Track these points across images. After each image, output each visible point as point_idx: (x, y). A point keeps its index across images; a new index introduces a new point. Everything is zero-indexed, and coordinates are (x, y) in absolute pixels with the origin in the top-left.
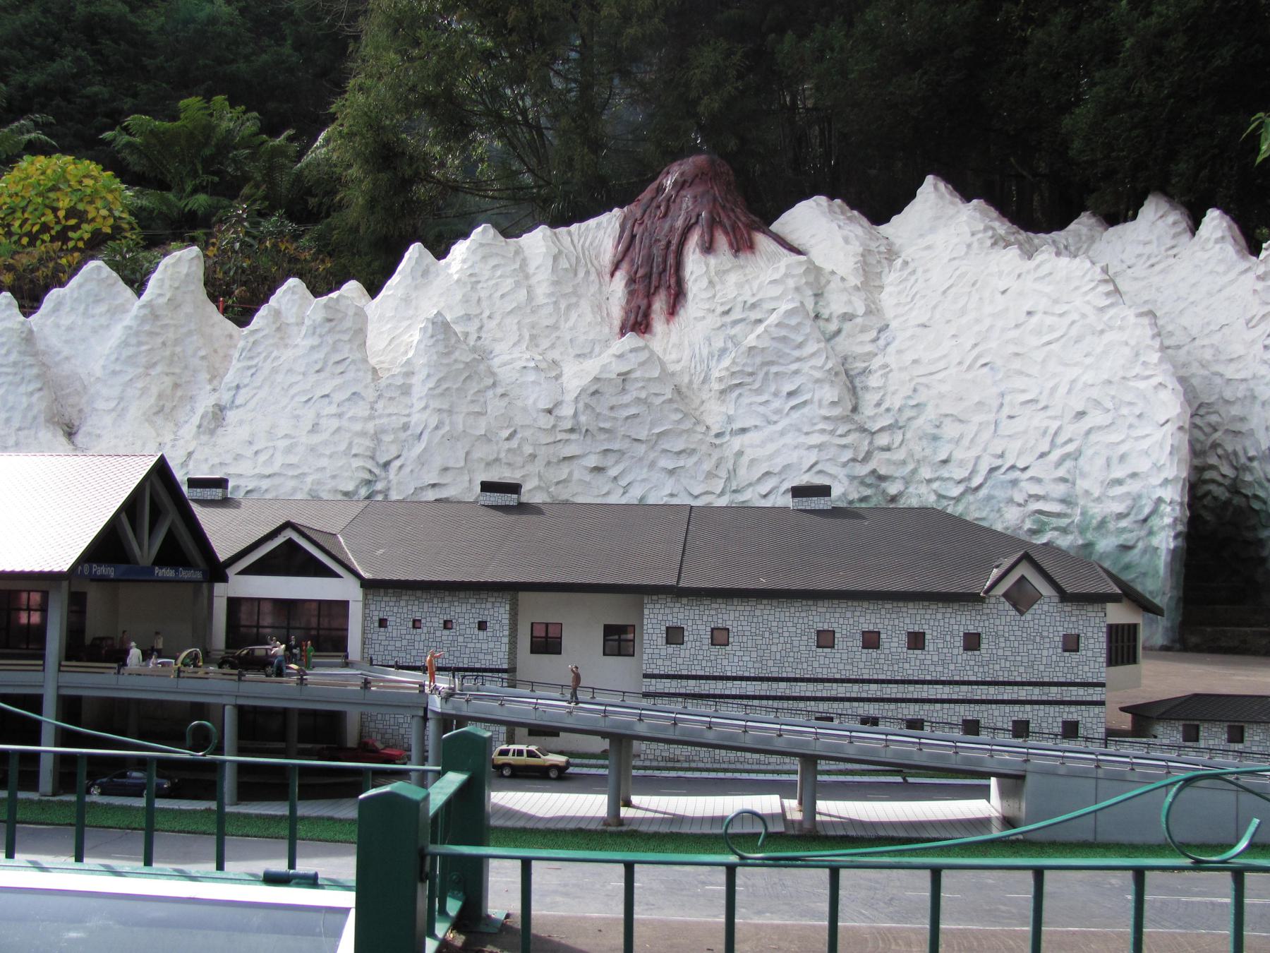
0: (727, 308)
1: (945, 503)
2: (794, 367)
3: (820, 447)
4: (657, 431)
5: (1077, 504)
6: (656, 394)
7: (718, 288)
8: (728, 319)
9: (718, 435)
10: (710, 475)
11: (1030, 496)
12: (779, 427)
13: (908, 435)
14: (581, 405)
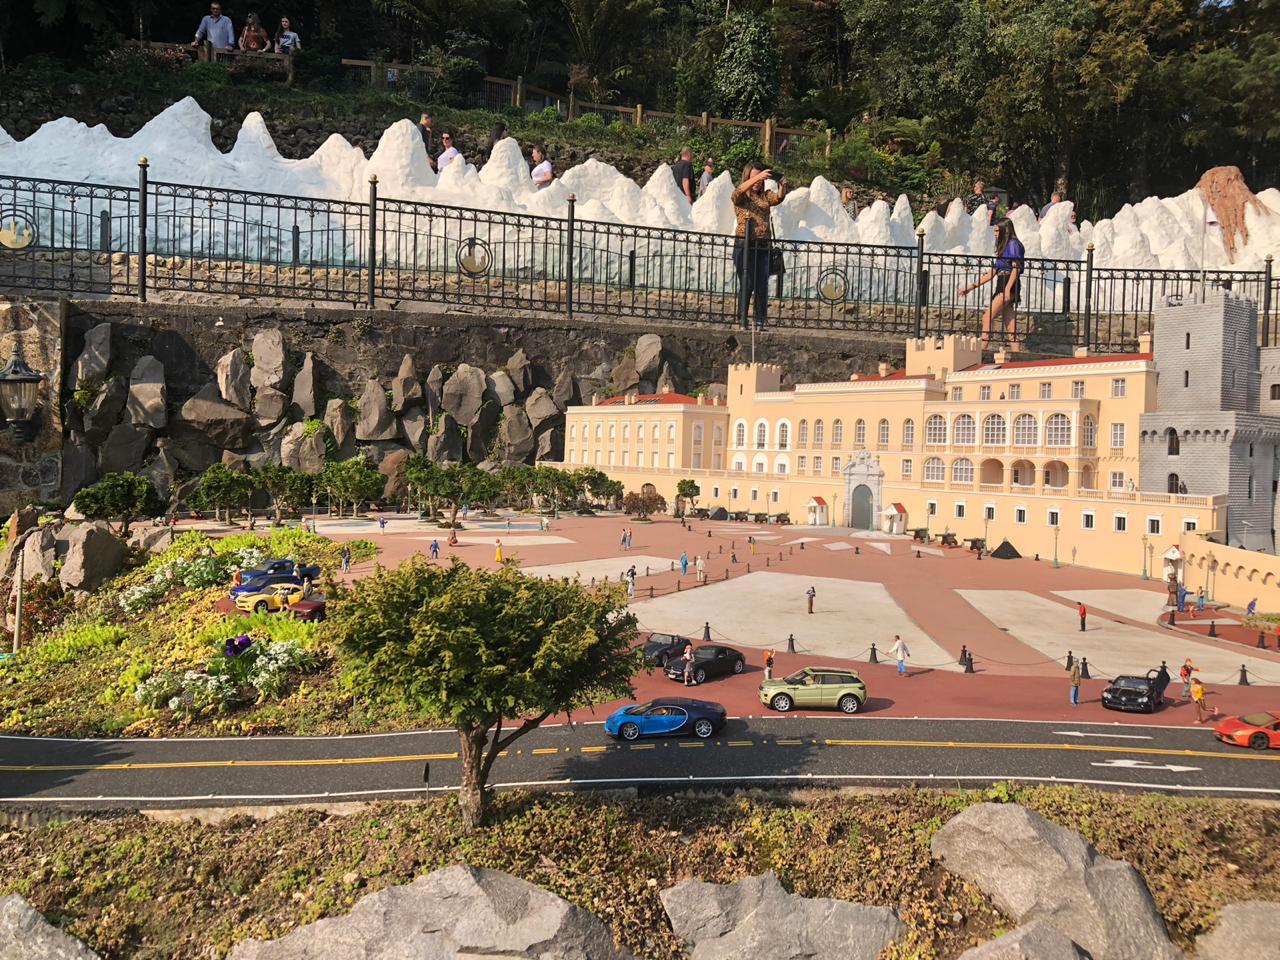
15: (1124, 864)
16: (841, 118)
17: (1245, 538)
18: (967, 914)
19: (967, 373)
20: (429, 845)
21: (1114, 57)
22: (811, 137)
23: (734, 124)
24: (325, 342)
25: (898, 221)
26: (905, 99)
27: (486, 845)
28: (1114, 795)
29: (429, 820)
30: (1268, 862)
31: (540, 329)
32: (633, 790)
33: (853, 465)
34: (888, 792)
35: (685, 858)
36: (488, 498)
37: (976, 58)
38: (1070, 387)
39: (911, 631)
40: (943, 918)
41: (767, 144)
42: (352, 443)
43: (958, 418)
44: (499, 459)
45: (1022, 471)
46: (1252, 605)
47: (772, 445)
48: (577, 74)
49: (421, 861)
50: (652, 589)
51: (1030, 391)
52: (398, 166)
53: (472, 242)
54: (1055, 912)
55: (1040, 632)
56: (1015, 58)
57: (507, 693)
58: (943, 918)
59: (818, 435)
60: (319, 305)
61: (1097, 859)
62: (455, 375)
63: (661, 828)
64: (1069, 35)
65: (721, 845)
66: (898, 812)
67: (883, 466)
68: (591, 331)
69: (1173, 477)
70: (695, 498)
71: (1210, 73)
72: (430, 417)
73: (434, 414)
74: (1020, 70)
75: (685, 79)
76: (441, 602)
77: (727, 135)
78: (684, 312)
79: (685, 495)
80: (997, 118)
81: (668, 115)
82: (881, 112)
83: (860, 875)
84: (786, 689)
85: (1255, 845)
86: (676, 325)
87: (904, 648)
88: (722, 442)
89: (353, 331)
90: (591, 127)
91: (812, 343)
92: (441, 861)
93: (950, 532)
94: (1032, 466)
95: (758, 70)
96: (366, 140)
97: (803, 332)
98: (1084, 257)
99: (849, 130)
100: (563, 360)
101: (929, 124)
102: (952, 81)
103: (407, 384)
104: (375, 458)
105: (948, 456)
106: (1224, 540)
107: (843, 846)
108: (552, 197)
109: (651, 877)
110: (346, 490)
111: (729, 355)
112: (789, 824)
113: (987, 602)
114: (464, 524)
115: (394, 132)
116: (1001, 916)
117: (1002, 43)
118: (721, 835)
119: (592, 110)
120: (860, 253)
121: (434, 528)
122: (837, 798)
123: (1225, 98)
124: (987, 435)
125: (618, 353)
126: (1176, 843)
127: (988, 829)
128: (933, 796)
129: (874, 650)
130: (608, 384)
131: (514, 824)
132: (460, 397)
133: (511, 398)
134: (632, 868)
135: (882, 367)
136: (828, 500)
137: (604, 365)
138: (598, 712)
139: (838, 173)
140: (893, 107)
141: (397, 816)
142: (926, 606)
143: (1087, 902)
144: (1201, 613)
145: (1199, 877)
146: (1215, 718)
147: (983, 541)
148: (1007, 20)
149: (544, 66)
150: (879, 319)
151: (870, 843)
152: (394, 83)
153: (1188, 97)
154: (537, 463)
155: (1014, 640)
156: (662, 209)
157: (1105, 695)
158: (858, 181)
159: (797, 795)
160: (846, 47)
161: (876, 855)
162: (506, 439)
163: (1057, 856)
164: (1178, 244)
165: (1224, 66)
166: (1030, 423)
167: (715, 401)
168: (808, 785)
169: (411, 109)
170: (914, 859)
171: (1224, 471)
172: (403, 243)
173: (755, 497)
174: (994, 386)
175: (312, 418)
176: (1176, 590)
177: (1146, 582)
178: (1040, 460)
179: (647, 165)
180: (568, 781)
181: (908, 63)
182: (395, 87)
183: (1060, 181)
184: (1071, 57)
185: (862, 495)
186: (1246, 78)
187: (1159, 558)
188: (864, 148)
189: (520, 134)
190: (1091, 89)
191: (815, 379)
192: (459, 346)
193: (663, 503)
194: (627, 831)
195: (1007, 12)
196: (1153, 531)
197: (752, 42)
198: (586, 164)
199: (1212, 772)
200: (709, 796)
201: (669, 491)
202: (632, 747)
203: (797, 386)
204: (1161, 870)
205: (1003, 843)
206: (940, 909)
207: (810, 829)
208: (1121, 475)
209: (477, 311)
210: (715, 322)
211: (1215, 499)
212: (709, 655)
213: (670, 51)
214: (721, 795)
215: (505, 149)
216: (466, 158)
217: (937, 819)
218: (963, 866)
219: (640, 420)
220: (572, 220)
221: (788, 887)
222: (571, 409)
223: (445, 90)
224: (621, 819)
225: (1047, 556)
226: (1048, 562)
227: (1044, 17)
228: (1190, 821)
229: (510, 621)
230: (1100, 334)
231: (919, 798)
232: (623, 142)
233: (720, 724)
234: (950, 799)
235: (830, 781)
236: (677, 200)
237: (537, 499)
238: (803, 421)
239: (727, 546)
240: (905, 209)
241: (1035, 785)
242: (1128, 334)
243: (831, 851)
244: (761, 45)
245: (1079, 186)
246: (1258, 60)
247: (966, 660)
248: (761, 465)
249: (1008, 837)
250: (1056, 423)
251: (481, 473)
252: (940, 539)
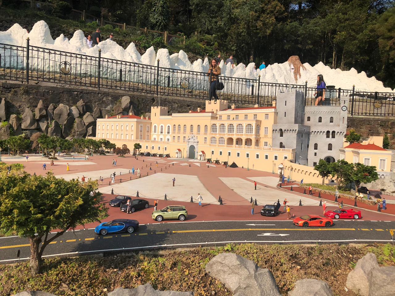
15: (267, 270)
16: (188, 33)
17: (300, 161)
18: (216, 291)
19: (223, 111)
20: (18, 282)
21: (266, 22)
22: (179, 38)
23: (155, 32)
24: (10, 95)
25: (205, 65)
26: (208, 29)
27: (40, 281)
28: (264, 246)
29: (19, 272)
30: (309, 265)
31: (88, 93)
32: (102, 255)
33: (190, 139)
34: (192, 249)
35: (119, 279)
36: (68, 149)
37: (228, 18)
38: (253, 116)
39: (204, 192)
40: (208, 294)
41: (166, 39)
42: (20, 130)
43: (221, 125)
44: (74, 136)
45: (239, 141)
46: (302, 181)
47: (165, 132)
48: (104, 11)
49: (13, 288)
50: (121, 180)
51: (242, 117)
52: (40, 36)
53: (65, 63)
54: (245, 288)
55: (244, 191)
56: (239, 19)
57: (44, 224)
58: (208, 294)
59: (179, 130)
60: (8, 82)
61: (258, 269)
62: (58, 107)
63: (111, 268)
64: (254, 14)
65: (132, 273)
66: (195, 256)
67: (198, 140)
68: (106, 94)
69: (281, 143)
70: (140, 149)
71: (291, 29)
72: (49, 121)
73: (50, 120)
74: (240, 23)
75: (140, 16)
76: (15, 190)
77: (153, 35)
78: (138, 90)
79: (137, 148)
80: (234, 37)
81: (134, 27)
82: (200, 32)
83: (181, 281)
84: (161, 214)
85: (305, 259)
86: (136, 93)
87: (201, 197)
88: (149, 131)
89: (21, 91)
90: (109, 29)
91: (178, 101)
92: (22, 288)
93: (218, 160)
94: (242, 140)
95: (163, 15)
96: (28, 26)
97: (176, 98)
98: (258, 79)
99: (191, 37)
100: (97, 103)
101: (215, 37)
102: (221, 24)
103: (41, 110)
104: (29, 135)
105: (217, 137)
106: (294, 162)
107: (176, 270)
108: (94, 51)
109: (105, 287)
110: (15, 146)
111: (152, 104)
112: (157, 263)
113: (227, 181)
114: (58, 158)
115: (38, 24)
116: (228, 291)
117: (236, 14)
118: (132, 269)
119: (109, 24)
120: (193, 74)
121: (47, 159)
122: (175, 252)
123: (295, 36)
124: (229, 130)
125: (115, 102)
126: (282, 261)
127: (224, 262)
128: (207, 250)
129: (192, 198)
130: (112, 112)
131: (52, 272)
132: (60, 115)
133: (78, 115)
134: (98, 285)
135: (199, 109)
136: (182, 150)
137: (111, 106)
138: (88, 228)
139: (187, 49)
140: (204, 31)
141: (6, 271)
142: (211, 185)
143: (255, 285)
144: (288, 183)
145: (289, 271)
146: (293, 217)
147: (227, 162)
148: (237, 8)
149: (93, 8)
150: (199, 95)
151: (185, 268)
152: (39, 8)
153: (286, 35)
154: (86, 137)
155: (236, 193)
156: (131, 57)
157: (262, 211)
158: (194, 53)
159: (161, 252)
160: (190, 11)
161: (187, 273)
162: (76, 129)
163: (246, 270)
164: (283, 77)
165: (296, 27)
166: (241, 127)
167: (147, 118)
168: (165, 248)
169: (45, 17)
170: (200, 273)
171: (295, 142)
172: (38, 62)
173: (159, 149)
174: (231, 116)
175: (5, 121)
176: (282, 177)
177: (273, 174)
178: (244, 138)
179: (127, 43)
180: (77, 252)
181: (208, 18)
182: (39, 9)
183: (251, 57)
184: (255, 20)
185: (192, 148)
186: (301, 31)
187: (277, 167)
188: (195, 43)
189: (84, 29)
190: (260, 30)
191: (179, 112)
192: (60, 98)
193: (129, 151)
194: (98, 270)
195: (237, 5)
196: (275, 159)
197: (161, 6)
198: (106, 40)
199: (293, 235)
200: (130, 255)
201: (131, 148)
202: (104, 238)
203: (173, 114)
204: (277, 270)
205: (229, 266)
206: (208, 291)
207: (164, 265)
208: (267, 142)
209: (67, 86)
210: (148, 93)
211: (292, 150)
212: (136, 203)
213: (135, 7)
214: (134, 254)
215: (78, 33)
216: (65, 36)
217: (208, 259)
218: (216, 275)
219: (122, 124)
220: (100, 58)
221: (155, 287)
222: (98, 120)
223: (57, 12)
224: (96, 266)
225: (246, 167)
226: (246, 168)
227: (247, 8)
228: (286, 253)
229: (47, 197)
230: (261, 102)
231: (202, 251)
232: (119, 35)
233: (137, 228)
234: (212, 251)
235: (173, 246)
236: (137, 54)
237: (86, 150)
238: (174, 125)
239: (149, 165)
240: (207, 62)
241: (240, 244)
242: (269, 102)
243: (171, 273)
244: (164, 8)
245: (256, 58)
246: (304, 26)
247: (220, 200)
248: (162, 139)
249: (231, 265)
250: (249, 127)
251: (66, 141)
252: (215, 162)
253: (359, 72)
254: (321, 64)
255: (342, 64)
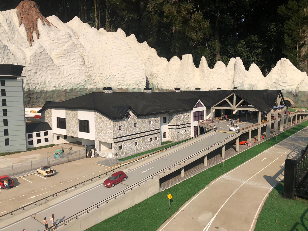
0: (53, 40)
1: (102, 81)
2: (74, 54)
3: (80, 70)
4: (48, 65)
5: (125, 81)
6: (48, 57)
7: (50, 34)
8: (53, 42)
9: (58, 66)
10: (58, 75)
11: (117, 80)
12: (71, 65)
13: (95, 69)
14: (32, 58)
253: (128, 35)
254: (76, 20)
255: (106, 23)
